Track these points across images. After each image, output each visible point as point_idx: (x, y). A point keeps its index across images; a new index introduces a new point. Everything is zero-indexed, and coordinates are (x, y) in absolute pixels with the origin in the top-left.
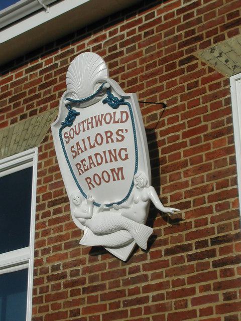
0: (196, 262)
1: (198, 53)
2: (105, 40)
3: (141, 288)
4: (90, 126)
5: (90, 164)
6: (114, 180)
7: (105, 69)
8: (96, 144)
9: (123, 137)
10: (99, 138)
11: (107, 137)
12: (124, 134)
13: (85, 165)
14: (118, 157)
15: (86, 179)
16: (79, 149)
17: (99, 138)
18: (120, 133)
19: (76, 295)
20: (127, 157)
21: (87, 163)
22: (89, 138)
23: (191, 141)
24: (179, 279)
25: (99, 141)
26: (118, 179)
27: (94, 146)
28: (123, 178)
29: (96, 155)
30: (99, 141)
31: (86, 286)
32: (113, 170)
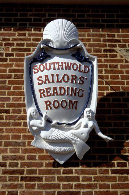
0: (118, 175)
1: (117, 49)
2: (45, 18)
3: (74, 185)
4: (61, 68)
5: (54, 92)
6: (70, 108)
7: (44, 35)
8: (63, 81)
9: (83, 82)
10: (66, 78)
12: (84, 81)
13: (49, 92)
14: (77, 94)
15: (46, 102)
16: (47, 80)
17: (66, 78)
18: (82, 79)
19: (14, 181)
20: (82, 96)
21: (52, 92)
22: (58, 75)
23: (14, 87)
25: (66, 80)
26: (73, 108)
27: (61, 82)
28: (76, 108)
29: (61, 88)
30: (66, 80)
31: (24, 175)
32: (70, 101)
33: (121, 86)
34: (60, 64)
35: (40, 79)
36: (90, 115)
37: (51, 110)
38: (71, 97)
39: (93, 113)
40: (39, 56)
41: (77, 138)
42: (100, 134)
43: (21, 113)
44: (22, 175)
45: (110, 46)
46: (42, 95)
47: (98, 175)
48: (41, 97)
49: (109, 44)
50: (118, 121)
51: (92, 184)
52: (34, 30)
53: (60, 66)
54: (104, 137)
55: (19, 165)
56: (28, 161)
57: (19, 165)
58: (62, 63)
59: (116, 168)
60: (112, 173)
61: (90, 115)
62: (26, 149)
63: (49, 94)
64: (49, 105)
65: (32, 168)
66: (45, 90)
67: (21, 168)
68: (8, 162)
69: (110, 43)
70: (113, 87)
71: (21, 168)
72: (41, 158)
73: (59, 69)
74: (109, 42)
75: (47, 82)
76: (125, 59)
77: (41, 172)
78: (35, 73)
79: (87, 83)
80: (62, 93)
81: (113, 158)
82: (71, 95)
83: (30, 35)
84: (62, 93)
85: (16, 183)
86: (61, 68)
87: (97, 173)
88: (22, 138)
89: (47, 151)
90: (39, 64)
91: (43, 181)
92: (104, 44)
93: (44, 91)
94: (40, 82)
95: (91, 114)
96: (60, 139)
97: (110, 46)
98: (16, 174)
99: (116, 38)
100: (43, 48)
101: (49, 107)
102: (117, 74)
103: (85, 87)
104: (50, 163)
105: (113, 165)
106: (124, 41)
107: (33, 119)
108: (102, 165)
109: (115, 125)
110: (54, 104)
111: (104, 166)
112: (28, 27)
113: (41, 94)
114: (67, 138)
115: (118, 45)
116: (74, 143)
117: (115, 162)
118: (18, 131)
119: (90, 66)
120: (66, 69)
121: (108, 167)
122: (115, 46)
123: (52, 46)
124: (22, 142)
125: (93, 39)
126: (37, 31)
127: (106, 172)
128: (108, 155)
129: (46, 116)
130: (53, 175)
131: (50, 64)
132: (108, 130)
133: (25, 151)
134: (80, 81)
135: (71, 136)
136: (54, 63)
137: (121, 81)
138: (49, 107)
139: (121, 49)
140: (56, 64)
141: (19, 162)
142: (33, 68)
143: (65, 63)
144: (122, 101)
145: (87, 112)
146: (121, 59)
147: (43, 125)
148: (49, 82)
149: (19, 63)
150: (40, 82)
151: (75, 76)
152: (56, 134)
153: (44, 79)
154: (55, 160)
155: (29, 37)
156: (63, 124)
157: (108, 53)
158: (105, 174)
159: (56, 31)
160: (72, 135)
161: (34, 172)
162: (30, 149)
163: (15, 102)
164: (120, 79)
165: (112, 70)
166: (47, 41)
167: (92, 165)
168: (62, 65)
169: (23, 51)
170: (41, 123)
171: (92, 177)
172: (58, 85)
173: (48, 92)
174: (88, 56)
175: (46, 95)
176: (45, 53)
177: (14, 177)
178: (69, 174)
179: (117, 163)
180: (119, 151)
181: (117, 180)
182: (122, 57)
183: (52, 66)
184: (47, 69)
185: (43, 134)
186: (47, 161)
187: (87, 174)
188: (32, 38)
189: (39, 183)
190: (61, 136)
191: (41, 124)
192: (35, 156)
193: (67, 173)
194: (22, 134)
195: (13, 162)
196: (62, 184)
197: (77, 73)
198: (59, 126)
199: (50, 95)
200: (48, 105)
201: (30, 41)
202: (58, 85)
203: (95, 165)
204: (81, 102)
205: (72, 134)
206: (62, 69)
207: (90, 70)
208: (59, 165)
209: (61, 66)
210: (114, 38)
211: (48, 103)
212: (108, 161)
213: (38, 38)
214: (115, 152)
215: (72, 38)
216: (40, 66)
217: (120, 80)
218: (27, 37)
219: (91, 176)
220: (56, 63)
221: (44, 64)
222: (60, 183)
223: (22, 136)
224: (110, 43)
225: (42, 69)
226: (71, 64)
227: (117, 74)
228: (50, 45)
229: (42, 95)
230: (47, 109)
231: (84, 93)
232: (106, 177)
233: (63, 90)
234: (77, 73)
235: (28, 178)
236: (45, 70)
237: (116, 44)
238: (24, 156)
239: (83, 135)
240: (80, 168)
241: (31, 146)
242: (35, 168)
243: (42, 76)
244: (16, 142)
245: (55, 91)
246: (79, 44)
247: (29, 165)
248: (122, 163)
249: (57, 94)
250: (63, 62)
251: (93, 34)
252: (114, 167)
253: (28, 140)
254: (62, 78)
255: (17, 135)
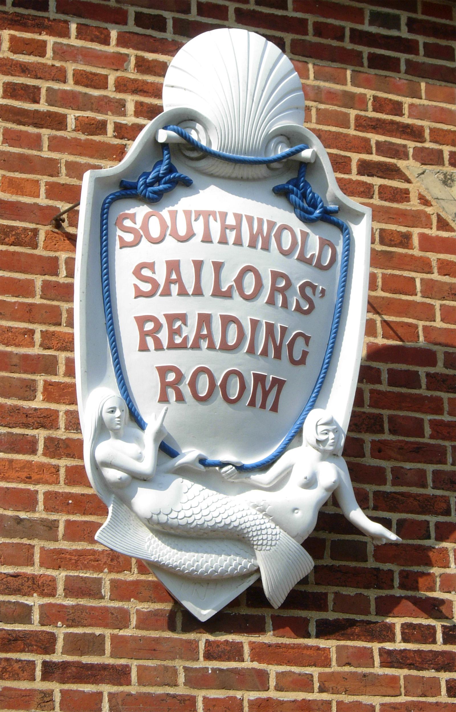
1: (409, 166)
3: (246, 704)
4: (231, 236)
5: (199, 337)
6: (252, 403)
8: (236, 294)
10: (250, 280)
11: (274, 289)
12: (316, 300)
13: (178, 331)
14: (285, 352)
15: (163, 371)
16: (174, 282)
17: (250, 280)
18: (308, 291)
20: (302, 361)
21: (190, 331)
22: (218, 267)
24: (360, 703)
26: (263, 406)
27: (228, 295)
28: (275, 408)
31: (57, 657)
32: (259, 379)
33: (421, 324)
34: (231, 221)
35: (146, 272)
36: (327, 440)
37: (180, 406)
38: (262, 361)
39: (336, 431)
40: (148, 174)
41: (273, 526)
42: (358, 516)
43: (33, 398)
44: (47, 658)
45: (382, 148)
46: (150, 342)
47: (335, 668)
48: (143, 348)
49: (378, 143)
50: (408, 466)
51: (314, 701)
52: (80, 36)
53: (228, 231)
54: (375, 528)
55: (36, 616)
56: (70, 602)
57: (36, 616)
58: (238, 217)
59: (399, 645)
60: (384, 664)
61: (327, 440)
62: (61, 552)
63: (178, 340)
64: (174, 385)
65: (88, 630)
66: (163, 321)
67: (44, 628)
68: (61, 632)
69: (382, 138)
70: (392, 325)
71: (44, 628)
72: (122, 591)
73: (223, 241)
74: (378, 133)
75: (175, 289)
76: (438, 215)
77: (121, 646)
78: (124, 245)
79: (324, 308)
80: (232, 340)
81: (387, 606)
82: (265, 353)
83: (61, 52)
84: (232, 340)
85: (24, 685)
86: (231, 236)
87: (330, 660)
88: (41, 506)
89: (145, 566)
90: (141, 211)
91: (129, 683)
92: (359, 137)
93: (158, 327)
94: (146, 287)
95: (331, 435)
96: (212, 523)
97: (382, 148)
98: (22, 651)
99: (406, 120)
100: (165, 146)
101: (172, 394)
102: (406, 274)
103: (316, 326)
104: (155, 613)
105: (386, 634)
106: (438, 136)
107: (109, 438)
108: (349, 631)
109: (399, 477)
110: (193, 384)
111: (358, 638)
112: (52, 13)
113: (144, 334)
114: (236, 524)
115: (411, 151)
116: (262, 545)
117: (397, 622)
118: (24, 475)
119: (341, 242)
120: (253, 245)
121: (371, 641)
122: (400, 153)
123: (204, 143)
124: (43, 521)
125: (318, 110)
126: (92, 40)
127: (364, 657)
128: (372, 594)
129: (160, 432)
130: (168, 663)
131: (188, 214)
132: (371, 496)
133: (56, 559)
134: (302, 302)
135: (251, 518)
136: (207, 215)
137: (423, 304)
138: (172, 394)
139: (425, 167)
140: (216, 220)
141: (35, 601)
142: (119, 223)
143: (250, 219)
144: (424, 386)
145: (317, 426)
146: (425, 213)
147: (146, 465)
148: (183, 292)
149: (17, 175)
150: (146, 287)
151: (283, 276)
152: (194, 503)
153: (160, 276)
154: (177, 603)
155: (58, 64)
156: (223, 465)
157: (376, 181)
158: (359, 666)
159: (225, 77)
160: (254, 511)
161: (95, 645)
162: (76, 550)
163: (9, 349)
164: (419, 294)
165: (391, 252)
166: (185, 119)
167: (312, 629)
168: (238, 227)
169: (36, 125)
170: (137, 453)
171: (312, 676)
172: (217, 309)
173: (173, 332)
174: (336, 200)
175: (165, 344)
176: (176, 164)
177: (18, 661)
178: (229, 660)
179: (404, 626)
180: (410, 581)
181: (403, 690)
182: (424, 201)
183: (198, 227)
184: (175, 234)
185: (145, 500)
186: (146, 607)
187: (296, 664)
188: (71, 67)
189: (114, 689)
190: (215, 514)
191: (139, 458)
192: (99, 581)
193: (219, 658)
194: (42, 489)
195: (9, 602)
196: (205, 698)
197: (291, 267)
198: (205, 471)
199: (183, 346)
200: (170, 384)
201: (65, 82)
202: (217, 309)
203: (326, 630)
204: (298, 382)
205: (255, 506)
206: (238, 242)
207: (339, 257)
208: (191, 623)
209: (231, 232)
210: (397, 119)
211: (171, 377)
212: (372, 618)
213: (95, 74)
214: (397, 582)
215: (283, 118)
216: (147, 218)
217: (418, 298)
218: (48, 59)
219: (308, 670)
220: (213, 213)
221: (165, 213)
222: (194, 692)
223: (41, 498)
224: (382, 138)
225: (155, 231)
226: (271, 224)
227: (406, 274)
228: (194, 135)
229: (150, 342)
230: (164, 399)
231: (311, 349)
232: (365, 676)
233: (233, 329)
234: (291, 267)
235: (74, 669)
236: (169, 240)
237: (405, 146)
238: (54, 580)
239: (298, 515)
240: (269, 638)
241: (96, 542)
242: (98, 631)
243: (153, 264)
244: (19, 521)
245: (205, 332)
246: (307, 147)
247: (72, 617)
248: (420, 625)
249: (211, 347)
250: (241, 216)
251: (319, 87)
252: (392, 640)
253: (68, 513)
254: (235, 281)
255: (22, 490)
